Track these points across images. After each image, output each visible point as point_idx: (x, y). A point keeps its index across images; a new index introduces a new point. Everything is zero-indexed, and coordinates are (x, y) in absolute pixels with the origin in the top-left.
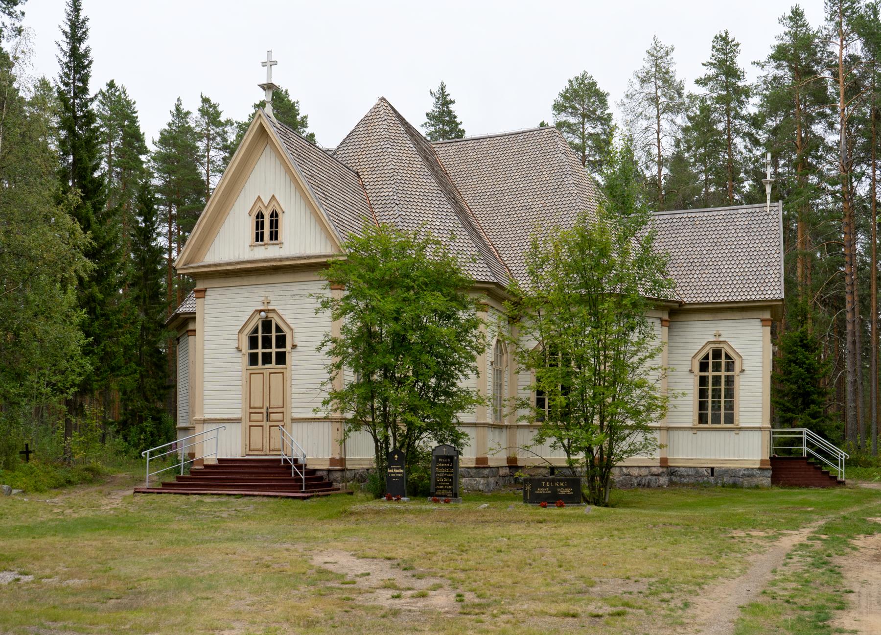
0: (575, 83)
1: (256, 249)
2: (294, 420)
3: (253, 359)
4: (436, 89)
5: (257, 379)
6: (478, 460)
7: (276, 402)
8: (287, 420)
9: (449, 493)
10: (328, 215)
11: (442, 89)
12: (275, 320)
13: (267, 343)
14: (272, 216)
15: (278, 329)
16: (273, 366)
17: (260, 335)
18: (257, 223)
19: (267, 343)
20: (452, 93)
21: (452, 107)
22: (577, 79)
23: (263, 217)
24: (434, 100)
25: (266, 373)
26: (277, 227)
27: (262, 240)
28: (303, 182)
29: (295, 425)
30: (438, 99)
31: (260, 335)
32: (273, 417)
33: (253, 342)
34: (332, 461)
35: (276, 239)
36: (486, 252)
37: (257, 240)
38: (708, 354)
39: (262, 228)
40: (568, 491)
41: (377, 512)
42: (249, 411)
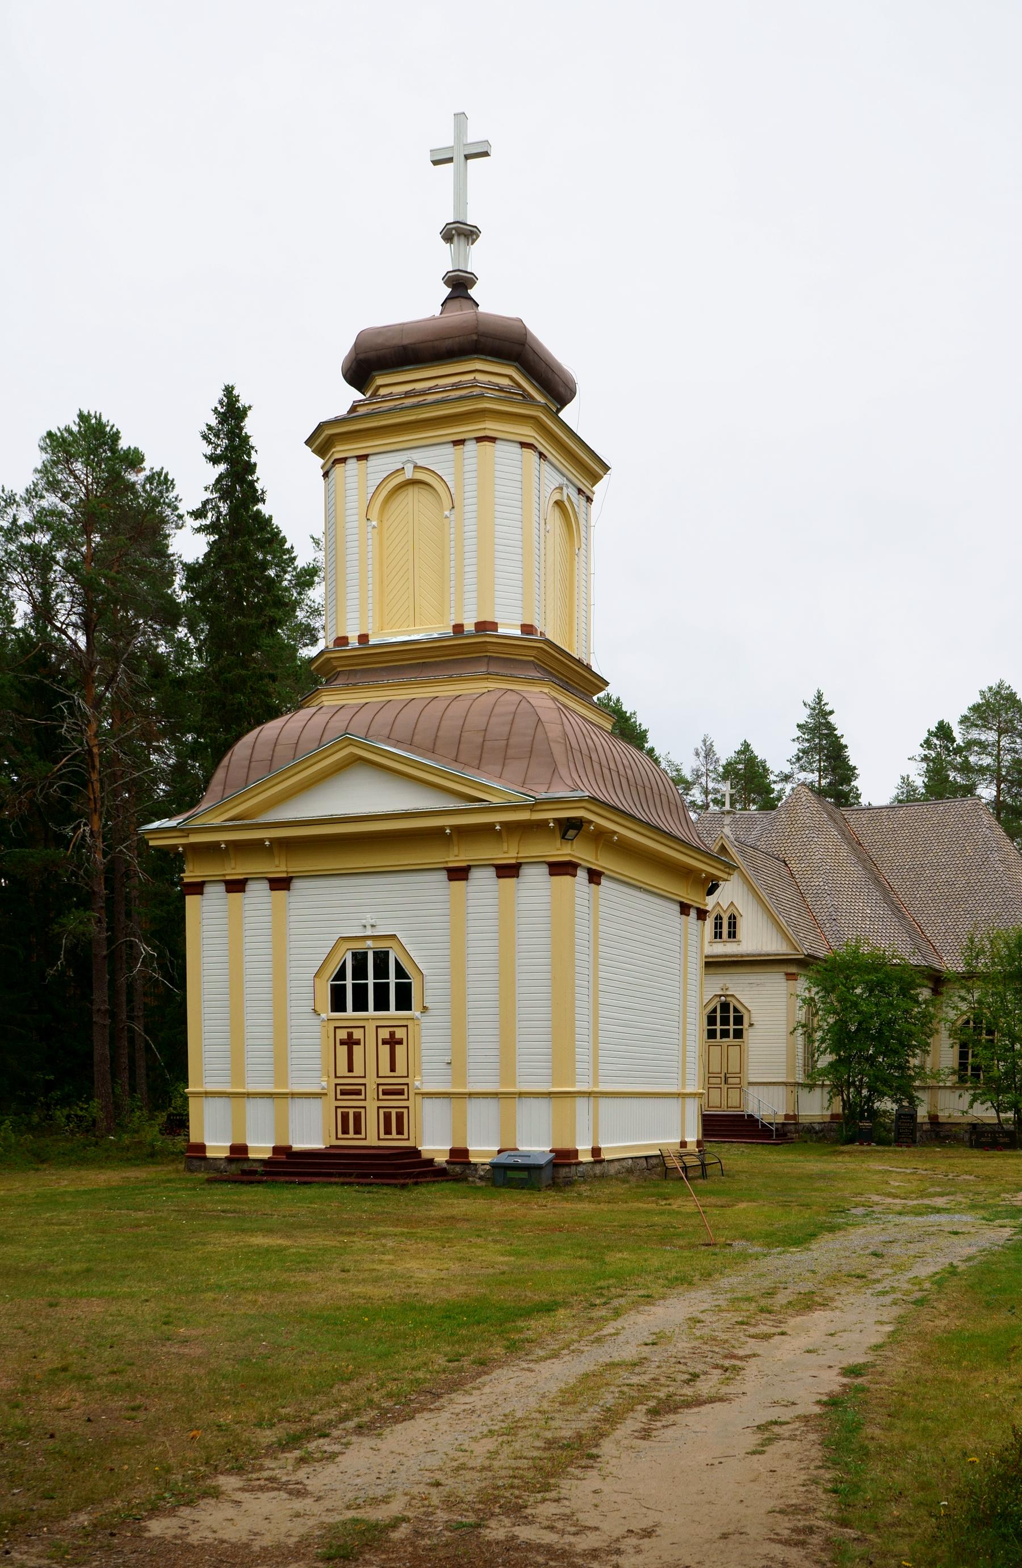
0: (988, 695)
1: (715, 945)
2: (750, 1084)
3: (712, 1034)
4: (810, 700)
5: (715, 1051)
6: (233, 1149)
7: (734, 1068)
8: (744, 1084)
9: (910, 1140)
10: (787, 921)
11: (818, 698)
12: (733, 1002)
13: (725, 1021)
14: (730, 918)
15: (400, 972)
16: (731, 1039)
17: (349, 982)
18: (716, 924)
19: (725, 1021)
20: (831, 702)
21: (831, 719)
22: (990, 689)
23: (721, 918)
24: (808, 711)
25: (725, 1046)
26: (735, 927)
27: (721, 937)
28: (763, 894)
29: (751, 1088)
30: (814, 709)
31: (349, 982)
32: (730, 1080)
33: (711, 1020)
34: (787, 1117)
35: (734, 937)
36: (916, 933)
37: (716, 937)
38: (343, 967)
39: (721, 928)
40: (1006, 1140)
41: (862, 1152)
42: (707, 1075)
